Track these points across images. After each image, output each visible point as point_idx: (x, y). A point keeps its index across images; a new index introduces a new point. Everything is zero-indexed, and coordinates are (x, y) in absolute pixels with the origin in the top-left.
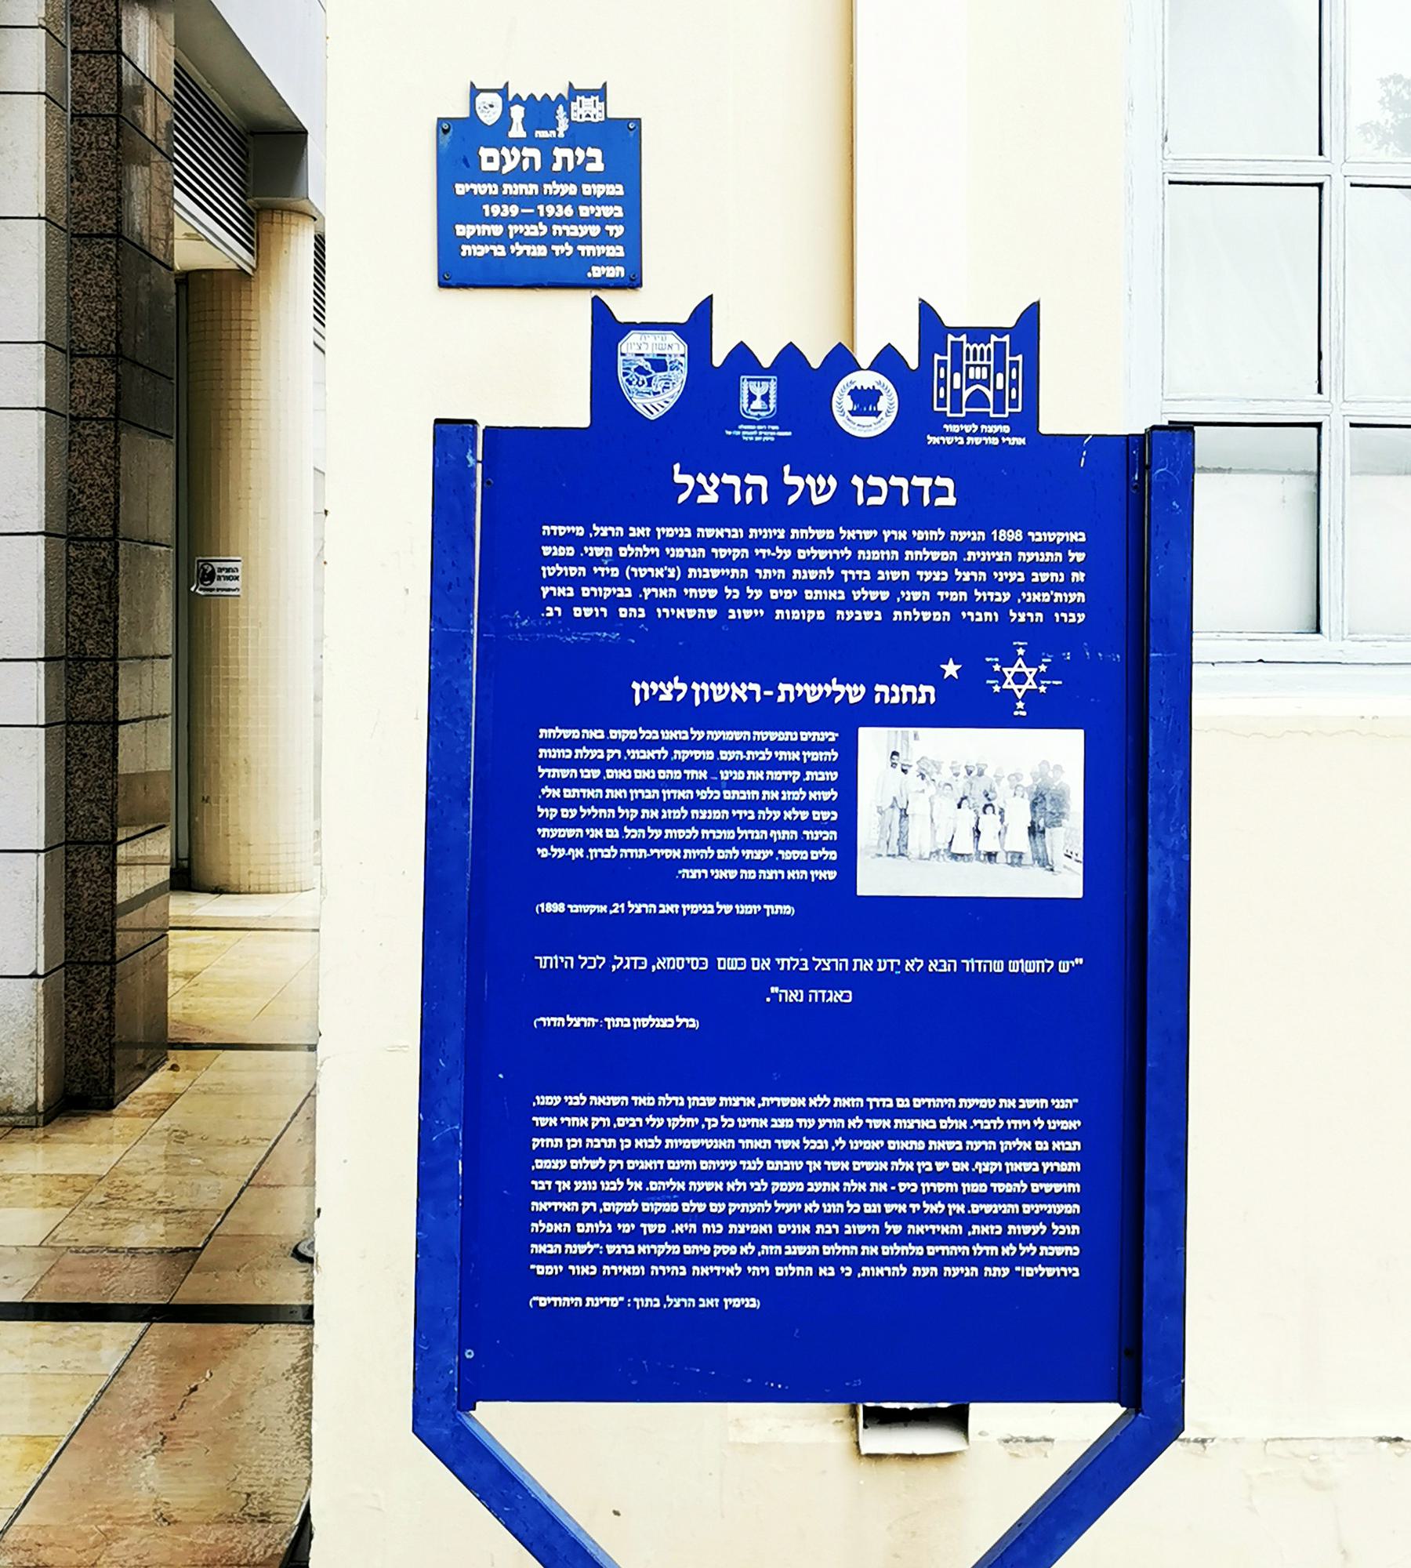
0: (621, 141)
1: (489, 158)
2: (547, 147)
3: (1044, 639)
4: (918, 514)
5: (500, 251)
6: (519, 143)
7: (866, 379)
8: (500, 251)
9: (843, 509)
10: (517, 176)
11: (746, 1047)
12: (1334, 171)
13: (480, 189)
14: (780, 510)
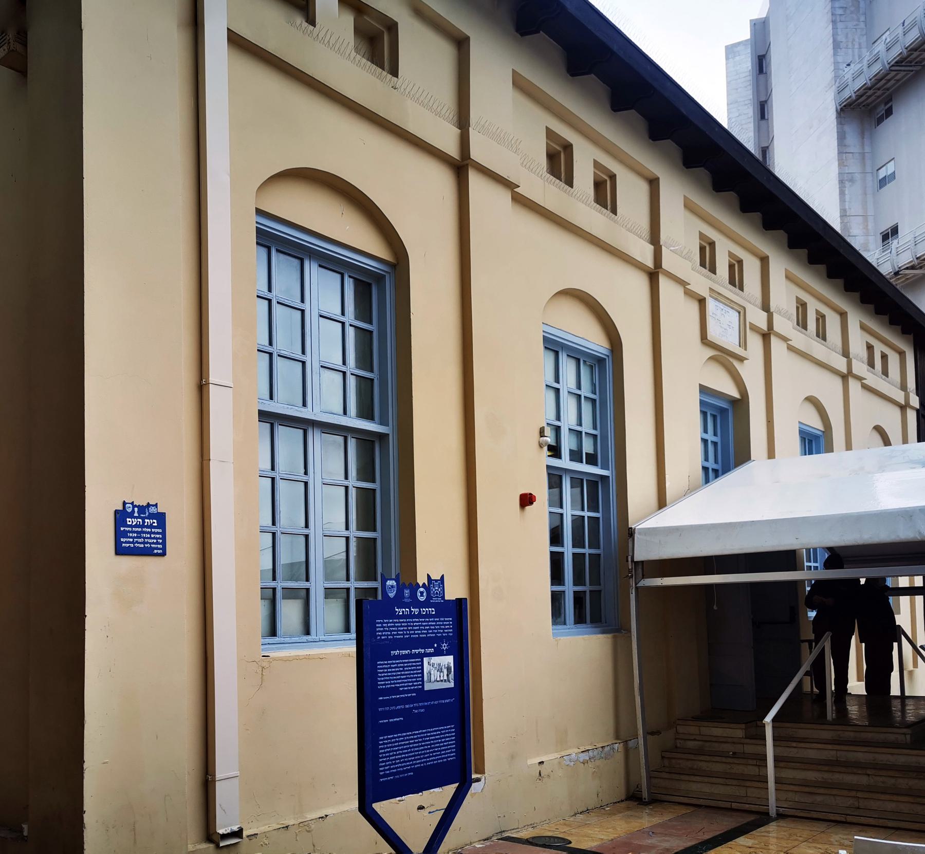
0: (161, 518)
2: (143, 519)
3: (448, 639)
4: (428, 616)
5: (132, 545)
6: (136, 518)
7: (422, 589)
8: (132, 545)
10: (136, 526)
11: (412, 723)
12: (278, 529)
13: (127, 529)
14: (411, 616)
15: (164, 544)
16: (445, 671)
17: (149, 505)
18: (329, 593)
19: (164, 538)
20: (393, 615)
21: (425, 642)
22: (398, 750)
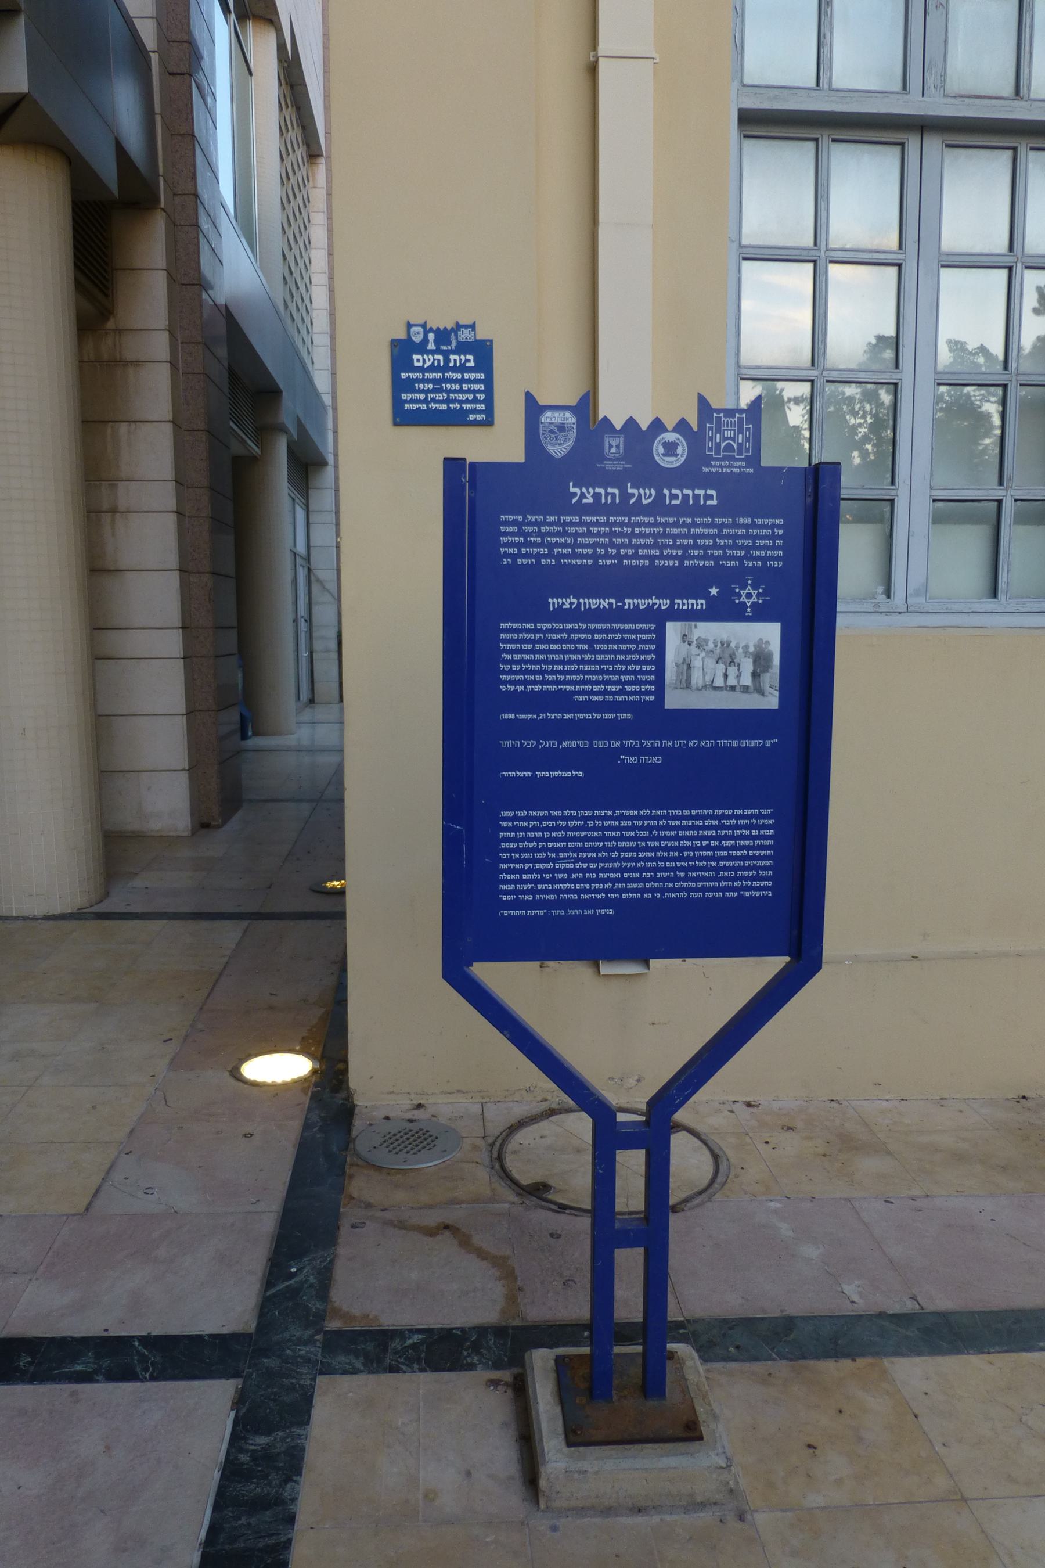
0: (483, 351)
1: (417, 360)
2: (446, 355)
3: (762, 576)
4: (698, 509)
5: (424, 407)
6: (433, 352)
7: (671, 437)
8: (424, 407)
9: (658, 506)
10: (432, 369)
11: (608, 785)
13: (414, 375)
14: (625, 507)
15: (489, 401)
16: (748, 666)
17: (459, 326)
18: (949, 512)
19: (489, 391)
20: (563, 504)
21: (682, 582)
22: (549, 853)
